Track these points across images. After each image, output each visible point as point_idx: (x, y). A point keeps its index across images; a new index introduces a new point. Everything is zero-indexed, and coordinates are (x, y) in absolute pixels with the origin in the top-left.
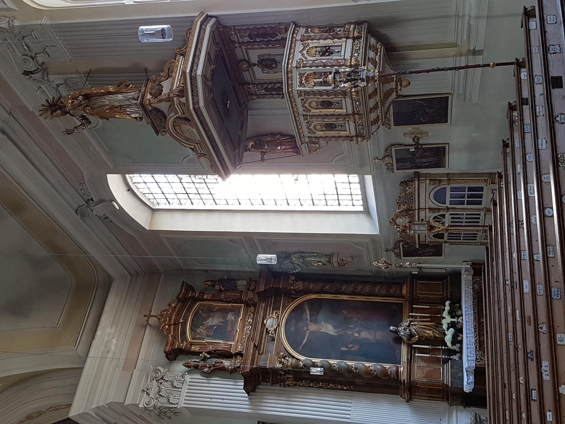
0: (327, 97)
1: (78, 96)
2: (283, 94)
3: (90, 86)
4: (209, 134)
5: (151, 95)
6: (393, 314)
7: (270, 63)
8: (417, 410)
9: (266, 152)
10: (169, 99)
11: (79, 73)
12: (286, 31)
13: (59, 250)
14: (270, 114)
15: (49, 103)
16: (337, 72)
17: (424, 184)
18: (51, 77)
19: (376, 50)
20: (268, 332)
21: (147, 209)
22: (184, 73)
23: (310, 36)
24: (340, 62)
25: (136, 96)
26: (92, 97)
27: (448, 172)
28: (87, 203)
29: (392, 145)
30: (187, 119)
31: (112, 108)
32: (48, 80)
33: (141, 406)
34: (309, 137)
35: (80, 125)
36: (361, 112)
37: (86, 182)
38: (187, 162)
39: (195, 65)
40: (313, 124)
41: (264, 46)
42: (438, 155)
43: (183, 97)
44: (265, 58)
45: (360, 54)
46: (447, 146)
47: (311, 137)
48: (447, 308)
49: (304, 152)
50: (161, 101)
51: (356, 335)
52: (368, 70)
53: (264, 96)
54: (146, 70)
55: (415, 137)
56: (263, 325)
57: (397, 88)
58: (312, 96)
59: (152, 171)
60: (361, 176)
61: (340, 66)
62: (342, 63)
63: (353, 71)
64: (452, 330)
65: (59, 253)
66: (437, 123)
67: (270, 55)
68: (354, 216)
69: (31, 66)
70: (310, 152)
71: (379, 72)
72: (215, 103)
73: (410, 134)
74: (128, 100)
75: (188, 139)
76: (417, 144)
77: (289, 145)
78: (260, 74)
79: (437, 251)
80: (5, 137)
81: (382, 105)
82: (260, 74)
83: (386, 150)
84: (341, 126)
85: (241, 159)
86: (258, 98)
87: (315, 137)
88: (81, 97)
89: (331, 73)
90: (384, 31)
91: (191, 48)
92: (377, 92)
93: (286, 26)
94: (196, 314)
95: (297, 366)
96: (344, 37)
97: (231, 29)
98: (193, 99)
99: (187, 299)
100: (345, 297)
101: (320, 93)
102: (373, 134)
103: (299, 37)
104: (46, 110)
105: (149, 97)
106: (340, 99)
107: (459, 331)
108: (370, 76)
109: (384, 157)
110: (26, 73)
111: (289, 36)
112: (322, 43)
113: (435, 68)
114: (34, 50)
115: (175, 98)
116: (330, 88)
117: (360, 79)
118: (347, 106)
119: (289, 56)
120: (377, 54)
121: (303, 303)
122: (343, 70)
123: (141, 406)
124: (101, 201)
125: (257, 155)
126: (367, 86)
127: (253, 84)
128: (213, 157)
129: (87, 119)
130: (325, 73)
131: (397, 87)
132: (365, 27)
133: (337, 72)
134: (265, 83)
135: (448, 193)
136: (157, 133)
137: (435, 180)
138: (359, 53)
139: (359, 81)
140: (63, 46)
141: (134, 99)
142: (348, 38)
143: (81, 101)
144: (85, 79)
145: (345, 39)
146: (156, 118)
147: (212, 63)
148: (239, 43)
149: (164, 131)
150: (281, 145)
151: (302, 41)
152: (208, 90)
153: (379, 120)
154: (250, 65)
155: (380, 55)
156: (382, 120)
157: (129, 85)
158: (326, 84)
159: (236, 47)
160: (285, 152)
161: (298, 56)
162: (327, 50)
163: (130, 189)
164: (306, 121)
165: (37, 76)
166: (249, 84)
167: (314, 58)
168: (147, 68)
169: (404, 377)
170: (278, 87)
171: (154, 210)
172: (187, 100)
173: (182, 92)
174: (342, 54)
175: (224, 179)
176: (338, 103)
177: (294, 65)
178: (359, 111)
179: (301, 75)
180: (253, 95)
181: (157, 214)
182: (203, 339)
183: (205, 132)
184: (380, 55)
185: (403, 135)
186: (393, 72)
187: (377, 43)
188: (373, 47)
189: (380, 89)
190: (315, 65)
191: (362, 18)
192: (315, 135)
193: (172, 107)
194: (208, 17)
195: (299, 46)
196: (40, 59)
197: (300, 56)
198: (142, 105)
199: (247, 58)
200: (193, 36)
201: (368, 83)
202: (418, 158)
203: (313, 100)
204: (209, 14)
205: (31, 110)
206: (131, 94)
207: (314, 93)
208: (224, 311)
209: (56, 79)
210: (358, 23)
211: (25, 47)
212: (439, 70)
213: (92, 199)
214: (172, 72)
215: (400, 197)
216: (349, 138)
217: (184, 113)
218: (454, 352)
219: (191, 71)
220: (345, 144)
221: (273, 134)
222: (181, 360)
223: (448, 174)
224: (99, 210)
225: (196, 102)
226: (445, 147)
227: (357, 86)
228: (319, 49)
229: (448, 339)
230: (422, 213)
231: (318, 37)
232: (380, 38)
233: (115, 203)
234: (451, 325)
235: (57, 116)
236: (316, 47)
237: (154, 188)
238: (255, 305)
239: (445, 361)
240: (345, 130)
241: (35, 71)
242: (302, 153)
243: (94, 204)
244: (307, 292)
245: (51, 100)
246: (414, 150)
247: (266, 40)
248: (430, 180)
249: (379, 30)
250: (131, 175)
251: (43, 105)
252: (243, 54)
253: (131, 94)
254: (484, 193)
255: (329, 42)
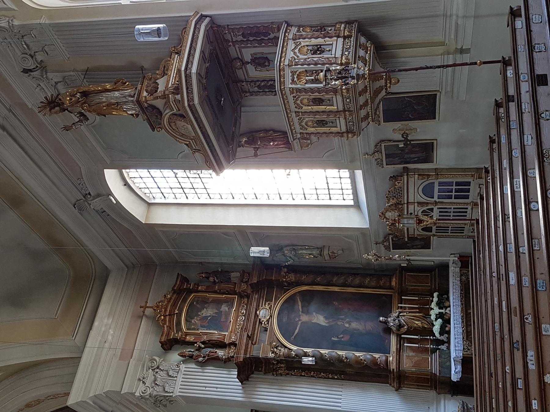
0: (318, 94)
1: (76, 94)
2: (275, 91)
3: (87, 84)
4: (204, 130)
5: (147, 92)
6: (383, 305)
7: (263, 62)
8: (406, 399)
9: (259, 148)
10: (165, 96)
11: (77, 71)
12: (279, 30)
13: (58, 243)
14: (263, 111)
15: (47, 100)
16: (328, 70)
17: (413, 179)
18: (50, 75)
19: (366, 49)
20: (260, 323)
21: (143, 203)
22: (179, 71)
23: (301, 35)
24: (331, 61)
25: (132, 93)
26: (89, 94)
27: (436, 167)
28: (84, 197)
29: (382, 141)
30: (182, 116)
31: (109, 105)
32: (46, 77)
33: (137, 394)
34: (300, 133)
35: (78, 122)
36: (351, 109)
37: (84, 177)
38: (182, 158)
39: (190, 63)
40: (305, 121)
41: (257, 45)
42: (426, 150)
43: (178, 94)
44: (258, 56)
45: (351, 53)
46: (435, 142)
47: (303, 133)
48: (435, 299)
49: (296, 147)
50: (156, 98)
51: (347, 325)
52: (358, 68)
53: (257, 93)
54: (142, 68)
55: (404, 133)
56: (256, 315)
57: (386, 86)
58: (304, 94)
59: (148, 166)
60: (351, 171)
61: (331, 64)
62: (333, 62)
63: (343, 69)
64: (440, 321)
65: (57, 246)
66: (425, 119)
67: (262, 53)
68: (344, 210)
69: (30, 64)
70: (301, 147)
71: (369, 70)
72: (209, 100)
73: (400, 130)
74: (125, 97)
75: (183, 135)
76: (406, 140)
77: (281, 141)
78: (253, 72)
79: (426, 244)
80: (5, 133)
81: (372, 102)
82: (253, 72)
83: (376, 146)
84: (332, 123)
85: (234, 155)
86: (251, 95)
87: (306, 133)
88: (79, 94)
89: (322, 71)
90: (374, 30)
91: (186, 47)
92: (367, 90)
93: (278, 25)
94: (191, 305)
95: (289, 356)
96: (335, 36)
97: (225, 28)
98: (188, 96)
99: (182, 290)
100: (336, 289)
101: (312, 90)
102: (363, 130)
103: (291, 36)
104: (45, 107)
105: (145, 94)
106: (331, 96)
107: (447, 322)
108: (360, 74)
109: (374, 153)
110: (26, 71)
111: (281, 35)
112: (314, 41)
113: (424, 66)
114: (33, 49)
115: (170, 95)
116: (321, 85)
117: (351, 77)
118: (338, 103)
119: (281, 54)
120: (367, 53)
121: (295, 295)
122: (334, 68)
123: (137, 394)
124: (99, 195)
125: (250, 151)
126: (357, 83)
127: (246, 82)
128: (207, 152)
129: (85, 116)
130: (316, 71)
131: (387, 85)
132: (355, 26)
133: (328, 70)
134: (258, 81)
135: (436, 188)
136: (153, 129)
137: (423, 175)
138: (349, 52)
139: (350, 79)
140: (61, 45)
141: (130, 96)
142: (338, 37)
143: (79, 99)
144: (83, 77)
145: (336, 38)
146: (152, 115)
147: (207, 62)
148: (232, 42)
149: (159, 127)
150: (273, 140)
151: (294, 39)
152: (203, 87)
153: (369, 117)
154: (243, 63)
155: (370, 54)
156: (372, 116)
157: (126, 83)
158: (317, 82)
159: (230, 46)
160: (277, 148)
161: (290, 55)
162: (318, 48)
163: (126, 184)
164: (298, 118)
165: (36, 74)
166: (243, 82)
167: (306, 57)
168: (143, 66)
169: (393, 366)
170: (271, 85)
171: (149, 204)
172: (182, 97)
173: (177, 90)
174: (333, 52)
175: (218, 174)
176: (329, 100)
177: (287, 63)
178: (350, 108)
179: (293, 73)
180: (246, 92)
181: (153, 208)
182: (198, 330)
183: (200, 128)
184: (370, 54)
185: (392, 131)
186: (382, 70)
187: (367, 42)
188: (364, 46)
189: (370, 87)
190: (306, 63)
191: (353, 17)
192: (307, 131)
193: (167, 103)
194: (203, 17)
195: (291, 45)
196: (39, 57)
197: (292, 54)
198: (139, 102)
199: (240, 57)
200: (188, 35)
201: (358, 81)
202: (407, 153)
203: (305, 97)
204: (204, 13)
205: (30, 107)
206: (128, 92)
207: (305, 90)
208: (218, 302)
209: (54, 77)
210: (349, 23)
211: (25, 46)
212: (427, 68)
213: (89, 194)
214: (167, 70)
215: (389, 192)
216: (340, 134)
217: (179, 110)
218: (442, 342)
219: (186, 69)
220: (336, 140)
221: (266, 131)
222: (177, 350)
223: (436, 169)
224: (96, 204)
225: (191, 100)
226: (433, 143)
227: (348, 83)
228: (310, 48)
229: (436, 329)
230: (411, 207)
231: (309, 36)
232: (370, 37)
233: (111, 198)
234: (439, 316)
235: (56, 113)
236: (307, 46)
237: (150, 183)
238: (248, 297)
239: (434, 351)
240: (336, 127)
241: (34, 69)
242: (294, 149)
243: (92, 198)
244: (299, 284)
245: (49, 97)
246: (403, 146)
247: (259, 39)
248: (418, 175)
249: (369, 29)
250: (128, 170)
251: (42, 102)
252: (237, 52)
253: (128, 92)
254: (471, 187)
255: (320, 41)
